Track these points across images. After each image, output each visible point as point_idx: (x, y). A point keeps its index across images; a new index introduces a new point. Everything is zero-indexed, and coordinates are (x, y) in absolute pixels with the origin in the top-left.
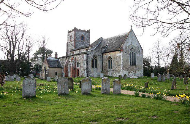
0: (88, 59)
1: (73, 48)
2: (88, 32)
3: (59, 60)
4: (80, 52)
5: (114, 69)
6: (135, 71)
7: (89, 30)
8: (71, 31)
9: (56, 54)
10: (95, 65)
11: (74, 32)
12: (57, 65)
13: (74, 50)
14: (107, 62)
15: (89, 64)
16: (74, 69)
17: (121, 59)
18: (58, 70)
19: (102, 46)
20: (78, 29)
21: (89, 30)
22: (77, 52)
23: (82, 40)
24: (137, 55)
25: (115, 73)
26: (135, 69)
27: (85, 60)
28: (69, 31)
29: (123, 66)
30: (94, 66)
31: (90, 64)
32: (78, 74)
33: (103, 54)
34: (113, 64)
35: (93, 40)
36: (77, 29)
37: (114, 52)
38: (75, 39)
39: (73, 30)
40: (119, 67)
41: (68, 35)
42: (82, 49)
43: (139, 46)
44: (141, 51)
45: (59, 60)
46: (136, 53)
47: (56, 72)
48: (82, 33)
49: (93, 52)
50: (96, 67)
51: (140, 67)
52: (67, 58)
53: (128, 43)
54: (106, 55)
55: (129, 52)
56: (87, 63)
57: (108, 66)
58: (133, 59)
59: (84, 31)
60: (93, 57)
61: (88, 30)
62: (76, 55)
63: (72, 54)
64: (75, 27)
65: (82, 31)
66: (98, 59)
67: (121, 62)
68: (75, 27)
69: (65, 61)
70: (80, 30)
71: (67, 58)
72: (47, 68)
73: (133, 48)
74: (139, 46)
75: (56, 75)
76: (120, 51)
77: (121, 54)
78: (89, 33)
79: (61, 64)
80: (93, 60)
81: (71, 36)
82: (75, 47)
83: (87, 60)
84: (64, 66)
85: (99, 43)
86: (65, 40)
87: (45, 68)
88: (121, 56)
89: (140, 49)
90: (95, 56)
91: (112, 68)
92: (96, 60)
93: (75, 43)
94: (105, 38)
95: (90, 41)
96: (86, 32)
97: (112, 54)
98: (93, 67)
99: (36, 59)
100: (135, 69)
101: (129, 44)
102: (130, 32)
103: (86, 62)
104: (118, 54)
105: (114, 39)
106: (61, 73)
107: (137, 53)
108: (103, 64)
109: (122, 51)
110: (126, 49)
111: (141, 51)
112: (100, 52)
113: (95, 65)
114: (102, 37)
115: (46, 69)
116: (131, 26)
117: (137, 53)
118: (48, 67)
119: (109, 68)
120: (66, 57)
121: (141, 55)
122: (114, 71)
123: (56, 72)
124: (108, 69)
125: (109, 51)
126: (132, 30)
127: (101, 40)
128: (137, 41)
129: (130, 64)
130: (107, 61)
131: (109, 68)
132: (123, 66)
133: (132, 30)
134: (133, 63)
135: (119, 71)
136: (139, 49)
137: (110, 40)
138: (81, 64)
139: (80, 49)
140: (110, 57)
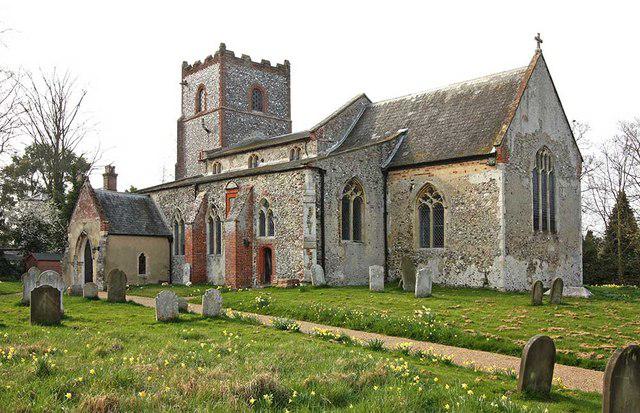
0: (322, 199)
1: (215, 143)
2: (284, 70)
3: (155, 197)
4: (253, 161)
5: (455, 248)
6: (554, 261)
7: (287, 62)
8: (198, 66)
9: (111, 175)
10: (351, 228)
11: (215, 68)
12: (144, 222)
13: (225, 156)
14: (415, 216)
15: (327, 220)
16: (245, 244)
18: (153, 248)
19: (374, 136)
21: (287, 63)
22: (241, 164)
25: (463, 268)
26: (552, 248)
27: (310, 199)
28: (191, 63)
29: (508, 237)
30: (428, 237)
31: (333, 223)
32: (267, 274)
33: (386, 172)
34: (446, 221)
35: (306, 114)
36: (232, 54)
37: (458, 167)
38: (223, 100)
39: (210, 60)
40: (496, 243)
41: (184, 84)
42: (270, 151)
44: (574, 164)
45: (155, 197)
46: (556, 174)
47: (142, 259)
48: (257, 77)
50: (357, 237)
52: (197, 189)
53: (528, 123)
54: (402, 181)
55: (532, 168)
56: (321, 217)
57: (416, 231)
58: (544, 205)
59: (265, 64)
60: (347, 189)
62: (268, 172)
63: (210, 174)
64: (223, 46)
65: (256, 65)
66: (366, 199)
67: (500, 216)
68: (223, 46)
69: (189, 207)
70: (245, 60)
71: (197, 189)
72: (98, 236)
73: (545, 148)
75: (142, 270)
76: (491, 160)
77: (498, 174)
78: (288, 77)
79: (166, 221)
80: (345, 202)
81: (201, 89)
82: (224, 141)
83: (321, 204)
84: (188, 228)
85: (355, 122)
86: (169, 104)
87: (83, 235)
88: (500, 184)
89: (572, 154)
90: (351, 183)
91: (439, 242)
92: (358, 202)
93: (223, 120)
94: (378, 97)
95: (289, 115)
97: (444, 176)
98: (345, 236)
99: (15, 197)
100: (553, 249)
101: (530, 128)
103: (314, 212)
104: (478, 174)
105: (438, 100)
106: (166, 262)
108: (390, 223)
109: (505, 161)
110: (519, 150)
111: (574, 164)
112: (375, 162)
113: (351, 228)
114: (364, 96)
115: (93, 244)
116: (539, 41)
118: (103, 233)
119: (425, 243)
120: (184, 182)
121: (574, 183)
122: (451, 257)
123: (142, 259)
125: (421, 158)
126: (540, 58)
127: (361, 109)
128: (560, 115)
129: (536, 227)
130: (415, 207)
133: (539, 52)
135: (483, 261)
137: (415, 107)
138: (290, 223)
139: (257, 149)
140: (429, 188)
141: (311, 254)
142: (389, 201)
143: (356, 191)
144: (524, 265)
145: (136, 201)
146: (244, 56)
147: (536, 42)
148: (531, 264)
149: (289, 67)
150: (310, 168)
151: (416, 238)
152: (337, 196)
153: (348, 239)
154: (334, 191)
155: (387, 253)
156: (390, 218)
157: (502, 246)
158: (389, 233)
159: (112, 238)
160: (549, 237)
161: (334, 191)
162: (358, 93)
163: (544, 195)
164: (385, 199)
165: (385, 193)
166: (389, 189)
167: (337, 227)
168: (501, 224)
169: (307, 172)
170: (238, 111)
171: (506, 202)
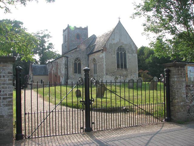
15: (69, 69)
26: (125, 73)
31: (71, 70)
33: (88, 55)
34: (127, 62)
46: (126, 53)
54: (92, 57)
55: (116, 52)
60: (76, 61)
61: (86, 27)
66: (82, 63)
68: (68, 25)
80: (75, 64)
89: (133, 47)
90: (77, 59)
92: (80, 64)
98: (76, 72)
100: (125, 73)
102: (118, 23)
103: (64, 67)
107: (128, 52)
109: (106, 51)
116: (119, 18)
117: (128, 52)
126: (119, 21)
131: (95, 74)
132: (106, 70)
133: (119, 21)
134: (122, 65)
141: (63, 77)
145: (42, 67)
148: (116, 77)
149: (87, 28)
150: (64, 56)
153: (77, 73)
157: (105, 73)
159: (34, 76)
162: (93, 34)
165: (88, 61)
166: (89, 60)
169: (63, 57)
171: (106, 62)
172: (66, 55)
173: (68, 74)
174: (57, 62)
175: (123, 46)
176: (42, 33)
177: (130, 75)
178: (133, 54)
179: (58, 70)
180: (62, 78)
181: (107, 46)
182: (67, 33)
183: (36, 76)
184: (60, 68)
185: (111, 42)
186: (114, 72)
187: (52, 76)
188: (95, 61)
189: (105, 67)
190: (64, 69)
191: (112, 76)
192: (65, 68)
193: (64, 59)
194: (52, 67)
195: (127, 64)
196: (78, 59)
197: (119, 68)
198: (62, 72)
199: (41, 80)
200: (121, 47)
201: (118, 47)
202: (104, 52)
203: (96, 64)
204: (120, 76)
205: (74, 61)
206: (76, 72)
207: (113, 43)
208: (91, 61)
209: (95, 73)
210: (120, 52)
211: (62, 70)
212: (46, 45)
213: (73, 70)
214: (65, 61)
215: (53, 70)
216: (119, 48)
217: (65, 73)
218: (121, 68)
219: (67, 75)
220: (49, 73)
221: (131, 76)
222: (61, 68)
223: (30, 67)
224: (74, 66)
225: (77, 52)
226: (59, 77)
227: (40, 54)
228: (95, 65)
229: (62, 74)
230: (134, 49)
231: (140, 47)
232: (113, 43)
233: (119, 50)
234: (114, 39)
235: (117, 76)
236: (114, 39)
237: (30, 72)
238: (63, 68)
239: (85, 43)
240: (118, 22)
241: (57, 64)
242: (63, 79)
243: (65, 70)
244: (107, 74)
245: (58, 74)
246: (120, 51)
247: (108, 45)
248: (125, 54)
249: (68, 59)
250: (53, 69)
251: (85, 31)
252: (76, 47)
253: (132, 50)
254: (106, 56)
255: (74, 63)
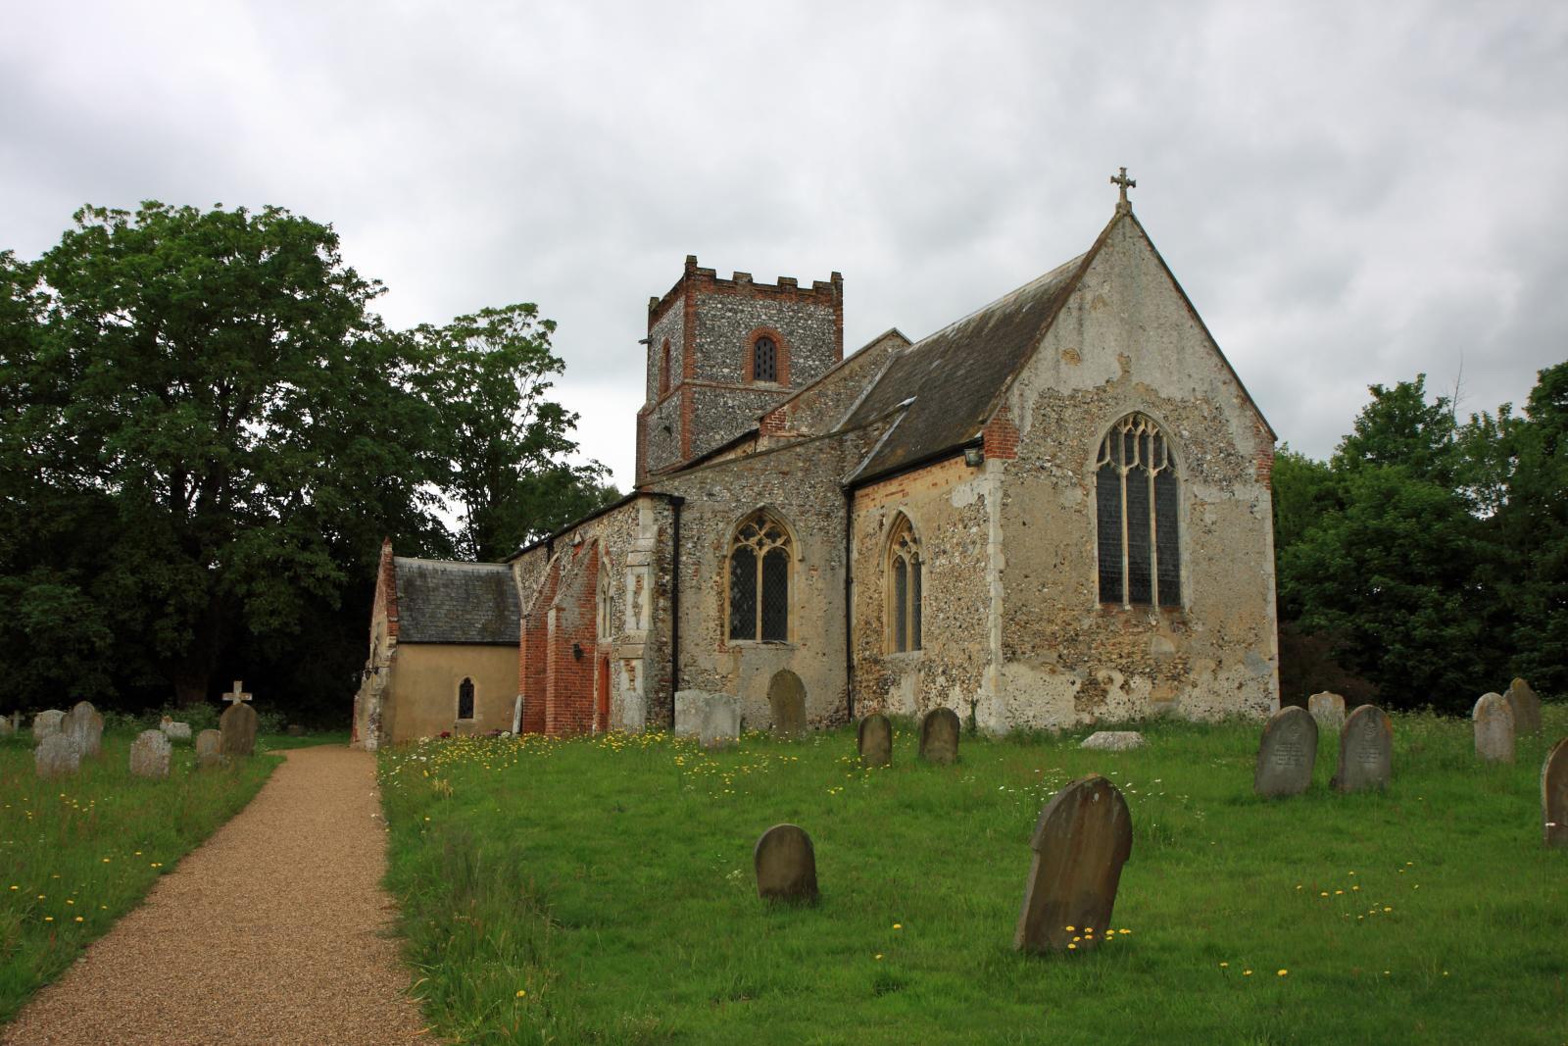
7: (837, 277)
15: (687, 599)
17: (984, 538)
20: (725, 274)
21: (837, 277)
23: (757, 376)
24: (1189, 492)
26: (1165, 644)
33: (851, 491)
34: (1185, 556)
36: (711, 274)
39: (676, 292)
43: (1227, 397)
46: (1181, 473)
47: (467, 689)
48: (764, 314)
49: (739, 477)
50: (776, 629)
51: (1234, 630)
55: (1093, 465)
57: (888, 618)
60: (745, 532)
64: (691, 262)
65: (765, 291)
66: (796, 551)
67: (991, 577)
68: (691, 262)
70: (742, 284)
73: (1136, 418)
74: (1227, 397)
75: (466, 710)
76: (972, 454)
78: (837, 305)
80: (743, 559)
89: (1237, 425)
90: (759, 516)
91: (918, 646)
92: (777, 564)
96: (803, 295)
98: (741, 629)
100: (1168, 646)
101: (1086, 377)
102: (1114, 224)
103: (648, 584)
108: (855, 599)
109: (1005, 452)
112: (823, 475)
116: (1124, 183)
117: (1197, 470)
119: (902, 647)
123: (467, 689)
124: (891, 655)
126: (1125, 213)
129: (1109, 591)
130: (887, 565)
131: (902, 647)
132: (1009, 617)
133: (1125, 213)
134: (1140, 580)
136: (1217, 420)
141: (632, 670)
142: (855, 555)
143: (772, 535)
144: (1066, 686)
145: (479, 577)
146: (737, 276)
147: (1116, 187)
150: (652, 496)
151: (889, 632)
152: (718, 547)
153: (753, 637)
154: (710, 538)
155: (850, 668)
156: (855, 589)
157: (994, 643)
158: (854, 621)
159: (408, 654)
160: (1156, 617)
161: (710, 538)
163: (1139, 526)
164: (848, 550)
167: (713, 612)
168: (992, 593)
169: (642, 503)
170: (718, 386)
171: (1005, 546)
172: (676, 487)
173: (676, 637)
174: (595, 543)
175: (1157, 414)
176: (492, 333)
177: (1213, 665)
178: (1237, 487)
179: (594, 608)
180: (625, 676)
181: (1022, 418)
182: (680, 325)
183: (417, 648)
184: (612, 592)
185: (1051, 383)
186: (1073, 640)
187: (551, 657)
188: (904, 544)
189: (995, 589)
190: (645, 598)
191: (1053, 672)
192: (659, 591)
193: (645, 529)
194: (555, 579)
195: (1184, 573)
196: (761, 523)
197: (1119, 599)
198: (630, 627)
199: (459, 682)
200: (1136, 424)
201: (1111, 424)
202: (994, 465)
203: (917, 566)
204: (1128, 671)
205: (729, 536)
206: (741, 629)
207: (1066, 392)
208: (869, 543)
209: (909, 642)
210: (1124, 470)
211: (629, 611)
212: (523, 418)
213: (721, 609)
214: (661, 532)
215: (559, 609)
216: (1114, 432)
217: (655, 630)
218: (1133, 600)
219: (668, 650)
220: (523, 633)
221: (1222, 675)
222: (621, 591)
223: (381, 575)
224: (733, 573)
225: (758, 464)
226: (606, 663)
227: (470, 485)
228: (907, 574)
229: (627, 640)
230: (1245, 446)
231: (1528, 392)
232: (1066, 392)
233: (1115, 449)
234: (1075, 357)
235: (1101, 675)
236: (1075, 357)
237: (380, 620)
238: (637, 593)
239: (821, 394)
240: (1111, 213)
241: (595, 558)
242: (639, 683)
243: (656, 609)
244: (1011, 654)
245: (594, 637)
246: (1129, 460)
247: (1031, 404)
248: (1167, 479)
249: (687, 516)
250: (556, 600)
251: (822, 312)
252: (756, 426)
253: (1229, 454)
254: (1006, 495)
255: (728, 550)
